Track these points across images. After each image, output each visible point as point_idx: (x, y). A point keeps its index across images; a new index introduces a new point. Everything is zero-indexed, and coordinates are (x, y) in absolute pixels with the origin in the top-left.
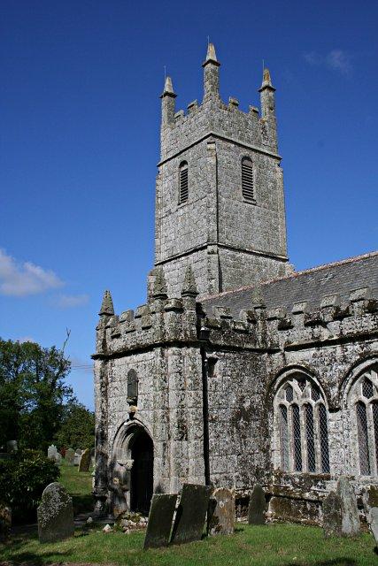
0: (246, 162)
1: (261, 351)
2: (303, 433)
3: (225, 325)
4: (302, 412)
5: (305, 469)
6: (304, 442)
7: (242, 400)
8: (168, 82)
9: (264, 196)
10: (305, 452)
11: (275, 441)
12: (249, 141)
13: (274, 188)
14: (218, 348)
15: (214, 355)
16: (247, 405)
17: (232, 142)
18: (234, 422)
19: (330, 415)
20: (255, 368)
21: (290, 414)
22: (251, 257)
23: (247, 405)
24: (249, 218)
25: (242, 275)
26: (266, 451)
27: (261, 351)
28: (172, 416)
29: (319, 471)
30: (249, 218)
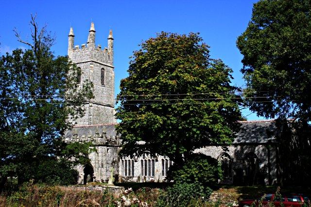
0: (103, 70)
1: (118, 146)
2: (128, 167)
3: (111, 140)
4: (127, 162)
5: (128, 175)
6: (128, 169)
7: (113, 159)
8: (71, 30)
9: (108, 83)
10: (128, 171)
11: (120, 169)
12: (104, 62)
13: (111, 80)
14: (109, 146)
15: (108, 148)
16: (114, 160)
17: (98, 63)
18: (112, 164)
19: (135, 163)
20: (116, 150)
21: (124, 162)
22: (103, 106)
23: (114, 160)
24: (102, 92)
25: (100, 113)
26: (118, 171)
27: (118, 146)
28: (100, 162)
29: (131, 176)
30: (102, 92)
